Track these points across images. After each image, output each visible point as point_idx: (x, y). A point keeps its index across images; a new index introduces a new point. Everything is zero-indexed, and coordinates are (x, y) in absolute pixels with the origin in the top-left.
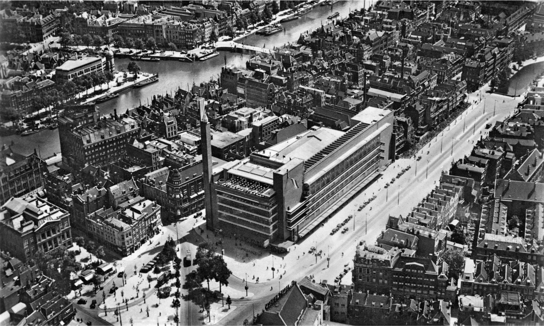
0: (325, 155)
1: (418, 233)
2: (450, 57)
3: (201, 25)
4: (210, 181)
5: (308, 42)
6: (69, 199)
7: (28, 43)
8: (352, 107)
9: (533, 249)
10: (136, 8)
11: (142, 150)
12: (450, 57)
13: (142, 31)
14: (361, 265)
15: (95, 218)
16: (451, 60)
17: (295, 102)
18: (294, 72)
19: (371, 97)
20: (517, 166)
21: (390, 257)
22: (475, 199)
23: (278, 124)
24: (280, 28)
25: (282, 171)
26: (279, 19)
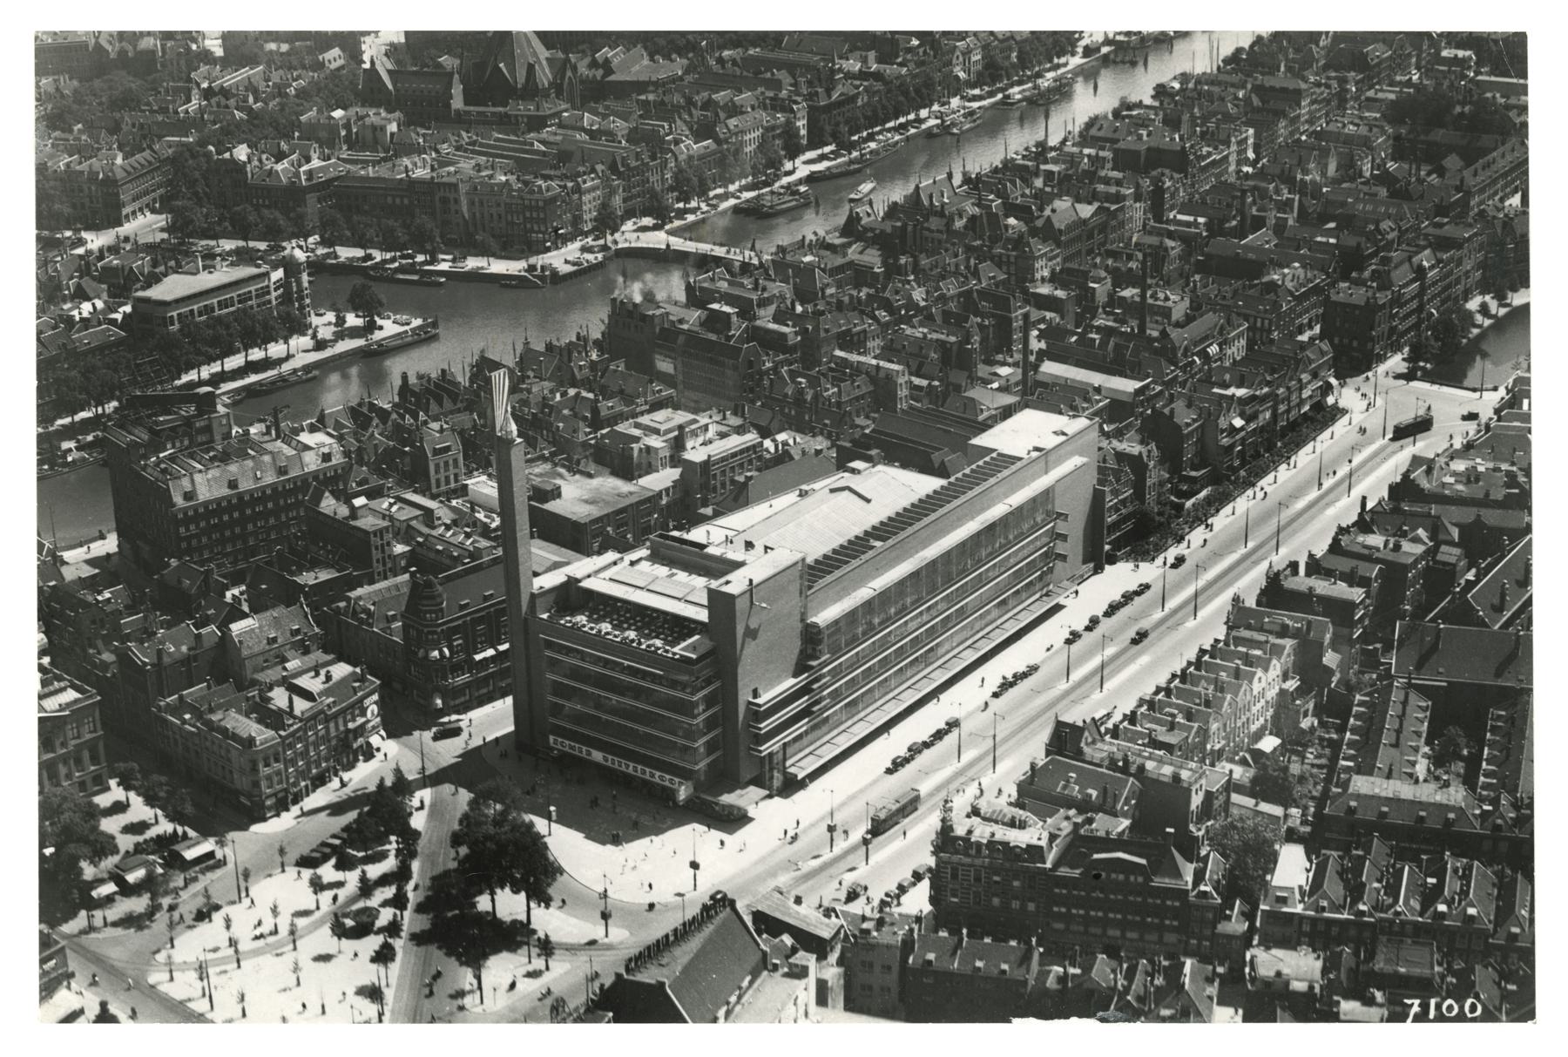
0: (878, 544)
1: (1142, 768)
2: (1289, 276)
3: (570, 185)
4: (524, 608)
5: (872, 230)
6: (108, 657)
7: (77, 231)
8: (986, 414)
9: (1499, 821)
10: (392, 134)
11: (343, 523)
12: (1289, 276)
13: (402, 197)
14: (956, 858)
15: (177, 710)
16: (1290, 285)
17: (816, 396)
18: (822, 313)
19: (1044, 385)
20: (1470, 585)
21: (1045, 835)
22: (1335, 679)
23: (760, 458)
24: (804, 195)
25: (735, 584)
26: (803, 171)
